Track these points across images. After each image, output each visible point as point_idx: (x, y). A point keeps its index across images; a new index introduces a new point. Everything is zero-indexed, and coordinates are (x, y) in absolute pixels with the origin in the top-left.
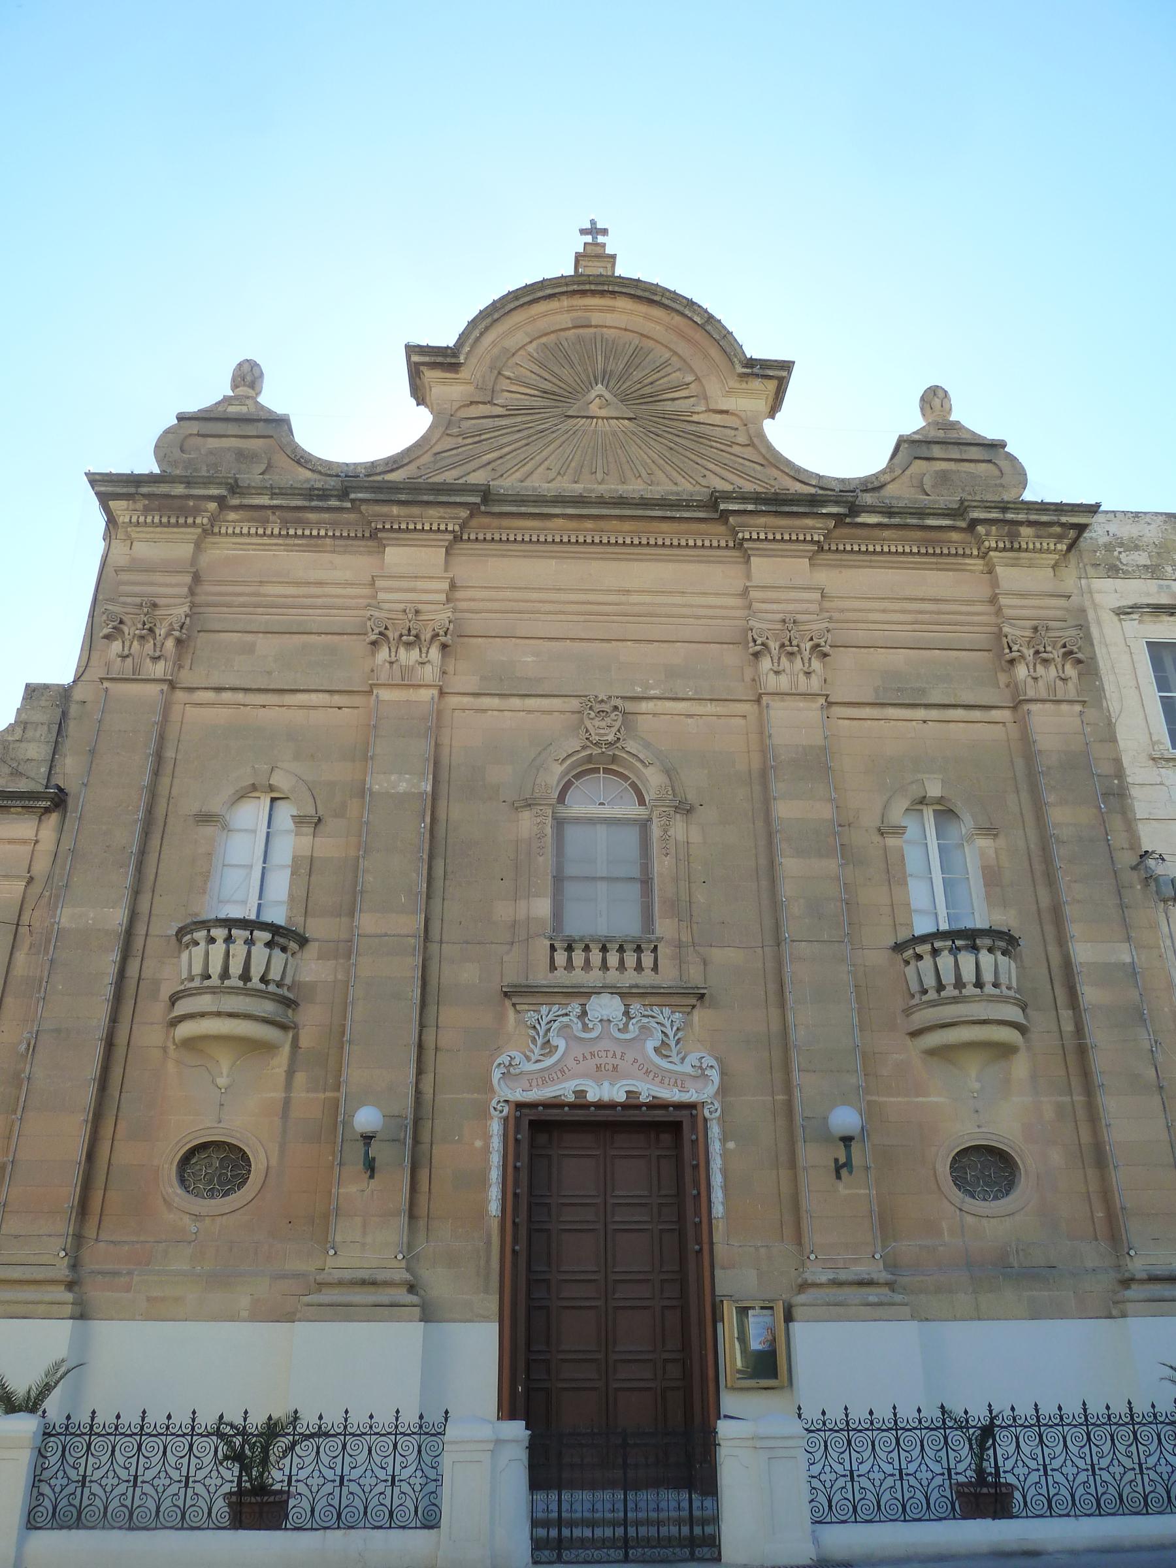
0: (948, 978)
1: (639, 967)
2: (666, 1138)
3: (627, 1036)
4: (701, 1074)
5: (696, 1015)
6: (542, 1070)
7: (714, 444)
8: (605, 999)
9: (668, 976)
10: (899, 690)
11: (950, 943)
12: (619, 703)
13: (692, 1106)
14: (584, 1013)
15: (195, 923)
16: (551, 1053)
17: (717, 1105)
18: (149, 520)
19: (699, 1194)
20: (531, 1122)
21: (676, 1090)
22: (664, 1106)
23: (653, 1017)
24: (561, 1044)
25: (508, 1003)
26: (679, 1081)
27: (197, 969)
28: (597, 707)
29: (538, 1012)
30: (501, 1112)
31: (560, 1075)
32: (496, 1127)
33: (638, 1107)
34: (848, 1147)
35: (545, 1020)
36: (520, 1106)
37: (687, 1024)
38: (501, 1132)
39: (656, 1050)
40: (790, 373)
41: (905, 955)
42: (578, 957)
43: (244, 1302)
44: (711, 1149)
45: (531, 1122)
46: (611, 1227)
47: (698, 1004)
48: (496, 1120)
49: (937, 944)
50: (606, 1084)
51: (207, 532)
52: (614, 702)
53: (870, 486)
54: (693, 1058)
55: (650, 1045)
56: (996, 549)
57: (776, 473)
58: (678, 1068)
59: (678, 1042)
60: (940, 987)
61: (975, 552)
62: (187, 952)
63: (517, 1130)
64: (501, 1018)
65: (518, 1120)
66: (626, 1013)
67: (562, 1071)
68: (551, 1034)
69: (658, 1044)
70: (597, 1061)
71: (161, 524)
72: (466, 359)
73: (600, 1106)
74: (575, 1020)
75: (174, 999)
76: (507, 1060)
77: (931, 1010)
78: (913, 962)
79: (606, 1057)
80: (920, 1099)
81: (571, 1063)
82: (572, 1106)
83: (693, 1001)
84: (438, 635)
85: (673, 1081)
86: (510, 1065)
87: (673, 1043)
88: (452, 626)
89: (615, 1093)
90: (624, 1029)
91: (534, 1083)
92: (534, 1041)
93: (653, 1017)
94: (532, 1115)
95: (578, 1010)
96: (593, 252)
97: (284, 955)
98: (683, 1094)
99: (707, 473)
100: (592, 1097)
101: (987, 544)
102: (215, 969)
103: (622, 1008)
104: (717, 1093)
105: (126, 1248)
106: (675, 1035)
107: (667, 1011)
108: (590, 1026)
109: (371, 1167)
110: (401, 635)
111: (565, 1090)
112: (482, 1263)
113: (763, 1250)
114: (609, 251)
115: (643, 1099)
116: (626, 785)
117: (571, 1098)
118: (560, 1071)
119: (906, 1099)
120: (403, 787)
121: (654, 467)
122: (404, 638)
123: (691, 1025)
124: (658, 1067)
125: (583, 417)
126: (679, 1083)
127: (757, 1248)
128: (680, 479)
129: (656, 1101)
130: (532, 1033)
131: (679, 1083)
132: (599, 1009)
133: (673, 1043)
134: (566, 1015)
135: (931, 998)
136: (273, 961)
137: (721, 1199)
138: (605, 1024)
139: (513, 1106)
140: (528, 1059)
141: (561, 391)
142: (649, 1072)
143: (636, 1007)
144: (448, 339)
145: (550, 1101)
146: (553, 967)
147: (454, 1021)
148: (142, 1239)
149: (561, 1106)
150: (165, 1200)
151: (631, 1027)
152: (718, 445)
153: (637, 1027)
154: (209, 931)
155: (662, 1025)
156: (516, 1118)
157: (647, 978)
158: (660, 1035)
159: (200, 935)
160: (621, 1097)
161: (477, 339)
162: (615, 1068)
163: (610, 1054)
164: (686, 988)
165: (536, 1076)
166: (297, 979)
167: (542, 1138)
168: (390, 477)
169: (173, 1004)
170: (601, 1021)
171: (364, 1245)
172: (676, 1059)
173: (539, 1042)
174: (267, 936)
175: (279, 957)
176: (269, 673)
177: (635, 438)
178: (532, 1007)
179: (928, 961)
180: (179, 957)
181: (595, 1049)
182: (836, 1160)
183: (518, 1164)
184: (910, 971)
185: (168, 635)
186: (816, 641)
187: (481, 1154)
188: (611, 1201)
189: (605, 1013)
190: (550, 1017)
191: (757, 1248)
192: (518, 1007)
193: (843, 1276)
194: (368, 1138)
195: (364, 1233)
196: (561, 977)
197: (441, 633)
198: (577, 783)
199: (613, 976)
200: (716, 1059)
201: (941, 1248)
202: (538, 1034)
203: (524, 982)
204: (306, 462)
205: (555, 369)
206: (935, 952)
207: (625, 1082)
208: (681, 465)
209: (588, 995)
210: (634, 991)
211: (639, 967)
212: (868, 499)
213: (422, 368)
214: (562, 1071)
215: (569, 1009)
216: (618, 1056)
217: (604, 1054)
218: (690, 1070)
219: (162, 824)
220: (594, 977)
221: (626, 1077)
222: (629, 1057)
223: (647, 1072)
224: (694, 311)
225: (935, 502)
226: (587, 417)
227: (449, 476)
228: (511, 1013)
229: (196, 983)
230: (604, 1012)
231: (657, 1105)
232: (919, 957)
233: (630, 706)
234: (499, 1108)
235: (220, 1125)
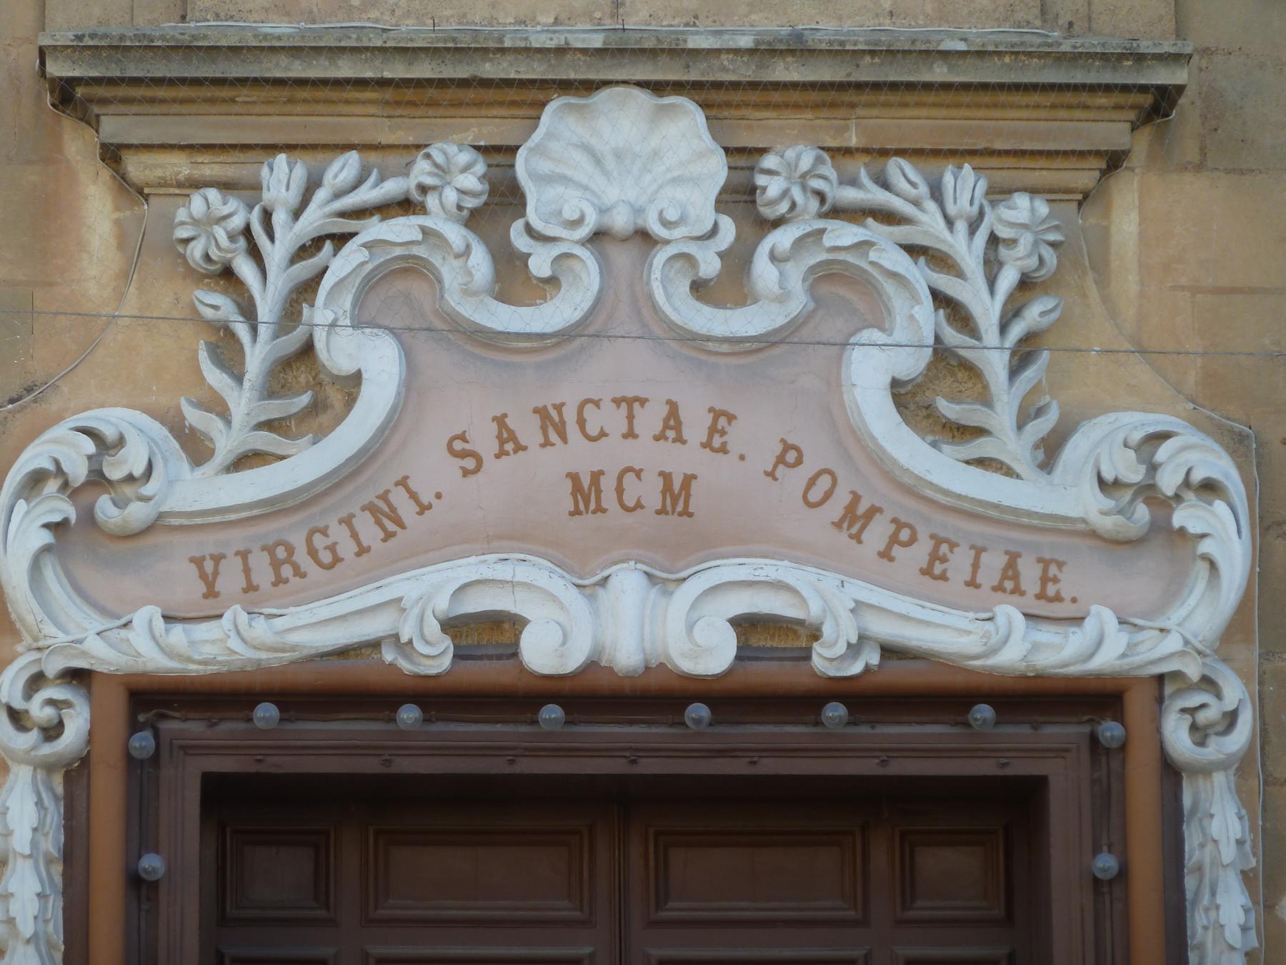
2: (953, 869)
4: (1152, 533)
5: (1127, 215)
6: (276, 507)
8: (622, 119)
13: (1096, 699)
14: (504, 198)
17: (1234, 691)
19: (1123, 874)
20: (220, 795)
21: (1009, 613)
22: (944, 696)
23: (888, 217)
24: (375, 360)
25: (77, 145)
26: (1031, 563)
29: (249, 189)
30: (52, 731)
31: (369, 531)
33: (806, 702)
35: (288, 235)
36: (150, 699)
37: (1076, 260)
38: (52, 843)
39: (905, 396)
44: (1198, 921)
45: (220, 795)
47: (1140, 145)
48: (22, 776)
50: (628, 582)
54: (1104, 443)
55: (870, 371)
58: (1028, 494)
59: (1022, 357)
63: (141, 827)
64: (46, 220)
65: (142, 775)
66: (739, 197)
67: (384, 513)
68: (319, 313)
69: (912, 364)
70: (578, 455)
73: (593, 696)
74: (455, 234)
76: (76, 457)
81: (431, 468)
82: (438, 699)
83: (1112, 131)
85: (993, 563)
86: (98, 480)
87: (995, 364)
89: (680, 627)
90: (729, 285)
91: (231, 579)
92: (227, 352)
93: (888, 217)
94: (222, 747)
95: (471, 179)
98: (1046, 634)
100: (547, 650)
103: (717, 170)
104: (1234, 630)
107: (964, 185)
108: (540, 264)
111: (401, 612)
115: (831, 659)
117: (434, 657)
118: (371, 513)
123: (1100, 266)
124: (913, 489)
126: (1029, 573)
129: (903, 675)
130: (217, 304)
131: (1029, 573)
132: (582, 168)
133: (995, 364)
134: (405, 205)
138: (622, 257)
139: (117, 705)
140: (196, 448)
142: (869, 517)
143: (790, 167)
145: (307, 677)
149: (379, 699)
151: (764, 271)
153: (796, 273)
156: (132, 763)
158: (926, 317)
160: (709, 651)
162: (677, 495)
163: (650, 419)
164: (1074, 58)
165: (236, 539)
167: (278, 874)
170: (599, 237)
172: (1012, 444)
173: (258, 355)
178: (210, 167)
181: (568, 393)
183: (152, 863)
189: (620, 201)
190: (315, 219)
192: (136, 167)
200: (1236, 443)
202: (248, 311)
203: (170, 29)
207: (729, 570)
209: (529, 96)
210: (784, 71)
214: (384, 513)
215: (422, 171)
216: (696, 428)
217: (614, 420)
218: (1085, 503)
222: (757, 433)
223: (855, 519)
228: (97, 208)
230: (612, 194)
234: (38, 710)
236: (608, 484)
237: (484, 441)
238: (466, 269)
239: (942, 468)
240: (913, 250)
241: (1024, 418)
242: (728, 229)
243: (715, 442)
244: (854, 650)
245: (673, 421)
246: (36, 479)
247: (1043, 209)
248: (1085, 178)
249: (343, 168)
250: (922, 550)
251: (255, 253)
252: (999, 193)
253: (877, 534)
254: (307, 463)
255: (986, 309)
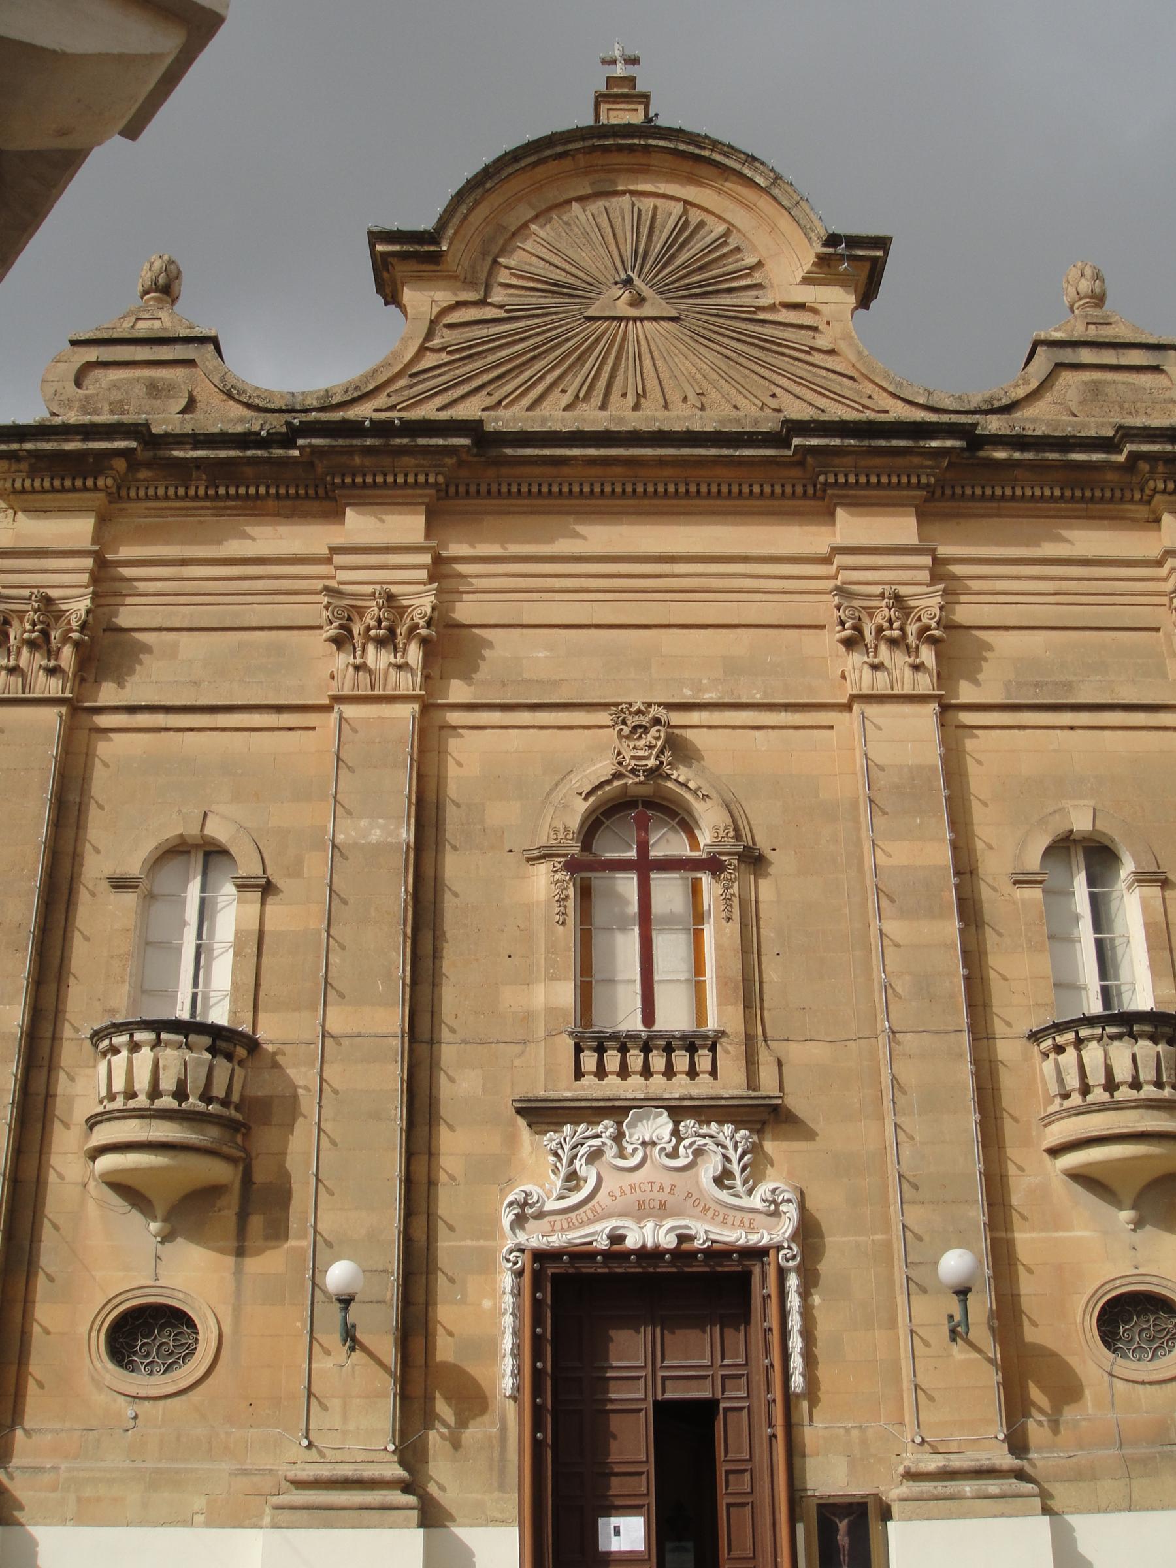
0: (1097, 1077)
1: (692, 1073)
3: (680, 1162)
7: (786, 351)
9: (730, 1082)
10: (1037, 684)
11: (1099, 1031)
12: (661, 713)
15: (114, 1025)
16: (577, 1188)
18: (37, 484)
23: (711, 1137)
27: (119, 1085)
28: (633, 722)
30: (515, 1263)
32: (507, 1280)
34: (964, 1302)
36: (541, 1256)
39: (718, 1181)
40: (886, 253)
41: (1043, 1046)
42: (612, 1060)
43: (199, 1503)
46: (660, 1374)
49: (1084, 1032)
51: (116, 496)
52: (654, 711)
53: (997, 404)
56: (1164, 491)
57: (869, 388)
58: (745, 1202)
59: (744, 1169)
60: (1085, 1090)
61: (1137, 496)
62: (105, 1062)
64: (512, 1140)
66: (675, 1132)
68: (577, 1163)
71: (53, 490)
72: (450, 244)
74: (609, 1142)
75: (93, 1122)
77: (1074, 1119)
78: (1052, 1056)
79: (651, 1190)
80: (1061, 1234)
84: (417, 626)
86: (526, 1204)
88: (436, 614)
90: (674, 1154)
92: (556, 1171)
96: (621, 91)
97: (229, 1065)
99: (778, 391)
100: (632, 1242)
101: (1151, 484)
102: (142, 1082)
103: (670, 1126)
105: (49, 1437)
106: (741, 1158)
107: (728, 1128)
109: (350, 1336)
110: (368, 629)
112: (496, 1454)
113: (855, 1433)
114: (640, 88)
116: (673, 823)
117: (603, 1244)
119: (1043, 1235)
120: (376, 836)
121: (705, 384)
122: (372, 633)
125: (607, 318)
127: (847, 1430)
128: (741, 401)
134: (598, 1136)
135: (1074, 1104)
136: (216, 1073)
137: (799, 1369)
141: (579, 283)
144: (426, 222)
146: (579, 1074)
147: (455, 1147)
148: (68, 1425)
150: (93, 1379)
151: (682, 1150)
152: (792, 353)
153: (690, 1151)
154: (132, 1035)
155: (724, 1147)
157: (703, 1087)
159: (121, 1040)
160: (668, 1242)
161: (465, 217)
163: (656, 1187)
166: (248, 1093)
168: (353, 413)
169: (91, 1128)
171: (345, 1433)
174: (206, 1040)
175: (223, 1068)
176: (196, 684)
177: (678, 344)
179: (1071, 1054)
180: (95, 1067)
182: (951, 1317)
184: (1048, 1066)
185: (65, 639)
186: (925, 620)
187: (487, 1323)
188: (660, 1374)
191: (847, 1430)
193: (957, 1462)
194: (346, 1302)
195: (345, 1418)
196: (590, 1088)
197: (422, 623)
198: (607, 823)
199: (658, 1085)
201: (1083, 1423)
204: (239, 393)
205: (570, 253)
206: (1079, 1043)
208: (743, 382)
211: (692, 1073)
212: (994, 425)
213: (390, 259)
215: (600, 1128)
219: (66, 892)
220: (634, 1087)
221: (678, 1214)
223: (705, 1210)
224: (756, 170)
225: (1084, 425)
226: (613, 318)
227: (428, 411)
229: (119, 1103)
231: (717, 1254)
232: (1060, 1049)
233: (676, 718)
234: (511, 1257)
235: (158, 1283)
236: (647, 1203)
237: (617, 1193)
238: (611, 1152)
239: (724, 1196)
240: (718, 1145)
241: (745, 1182)
242: (674, 1140)
243: (672, 1192)
244: (704, 1242)
245: (661, 1187)
246: (511, 1204)
247: (748, 1133)
248: (759, 1127)
249: (582, 1127)
250: (721, 1217)
251: (562, 1147)
252: (737, 1130)
253: (710, 1213)
254: (575, 1198)
255: (734, 1158)
